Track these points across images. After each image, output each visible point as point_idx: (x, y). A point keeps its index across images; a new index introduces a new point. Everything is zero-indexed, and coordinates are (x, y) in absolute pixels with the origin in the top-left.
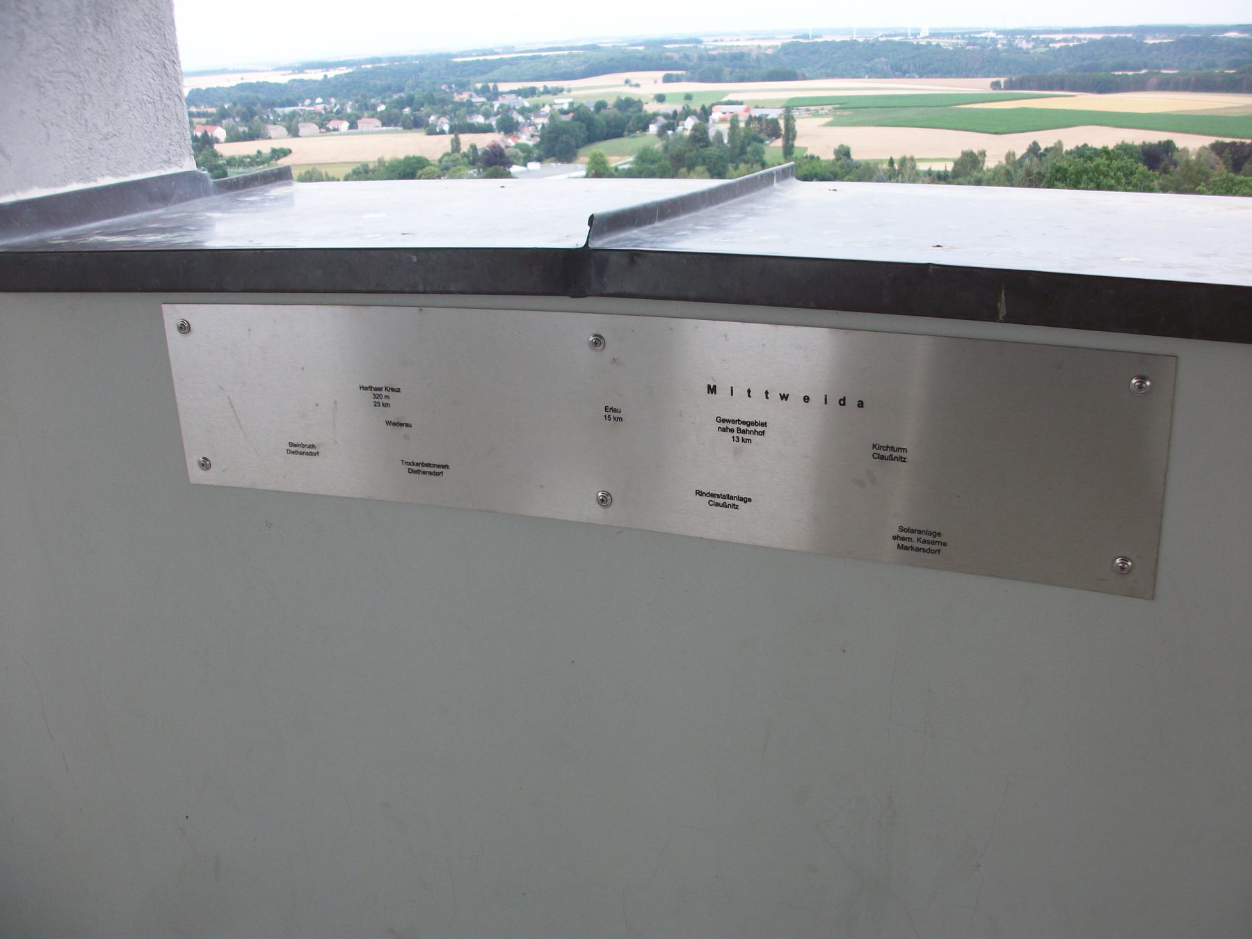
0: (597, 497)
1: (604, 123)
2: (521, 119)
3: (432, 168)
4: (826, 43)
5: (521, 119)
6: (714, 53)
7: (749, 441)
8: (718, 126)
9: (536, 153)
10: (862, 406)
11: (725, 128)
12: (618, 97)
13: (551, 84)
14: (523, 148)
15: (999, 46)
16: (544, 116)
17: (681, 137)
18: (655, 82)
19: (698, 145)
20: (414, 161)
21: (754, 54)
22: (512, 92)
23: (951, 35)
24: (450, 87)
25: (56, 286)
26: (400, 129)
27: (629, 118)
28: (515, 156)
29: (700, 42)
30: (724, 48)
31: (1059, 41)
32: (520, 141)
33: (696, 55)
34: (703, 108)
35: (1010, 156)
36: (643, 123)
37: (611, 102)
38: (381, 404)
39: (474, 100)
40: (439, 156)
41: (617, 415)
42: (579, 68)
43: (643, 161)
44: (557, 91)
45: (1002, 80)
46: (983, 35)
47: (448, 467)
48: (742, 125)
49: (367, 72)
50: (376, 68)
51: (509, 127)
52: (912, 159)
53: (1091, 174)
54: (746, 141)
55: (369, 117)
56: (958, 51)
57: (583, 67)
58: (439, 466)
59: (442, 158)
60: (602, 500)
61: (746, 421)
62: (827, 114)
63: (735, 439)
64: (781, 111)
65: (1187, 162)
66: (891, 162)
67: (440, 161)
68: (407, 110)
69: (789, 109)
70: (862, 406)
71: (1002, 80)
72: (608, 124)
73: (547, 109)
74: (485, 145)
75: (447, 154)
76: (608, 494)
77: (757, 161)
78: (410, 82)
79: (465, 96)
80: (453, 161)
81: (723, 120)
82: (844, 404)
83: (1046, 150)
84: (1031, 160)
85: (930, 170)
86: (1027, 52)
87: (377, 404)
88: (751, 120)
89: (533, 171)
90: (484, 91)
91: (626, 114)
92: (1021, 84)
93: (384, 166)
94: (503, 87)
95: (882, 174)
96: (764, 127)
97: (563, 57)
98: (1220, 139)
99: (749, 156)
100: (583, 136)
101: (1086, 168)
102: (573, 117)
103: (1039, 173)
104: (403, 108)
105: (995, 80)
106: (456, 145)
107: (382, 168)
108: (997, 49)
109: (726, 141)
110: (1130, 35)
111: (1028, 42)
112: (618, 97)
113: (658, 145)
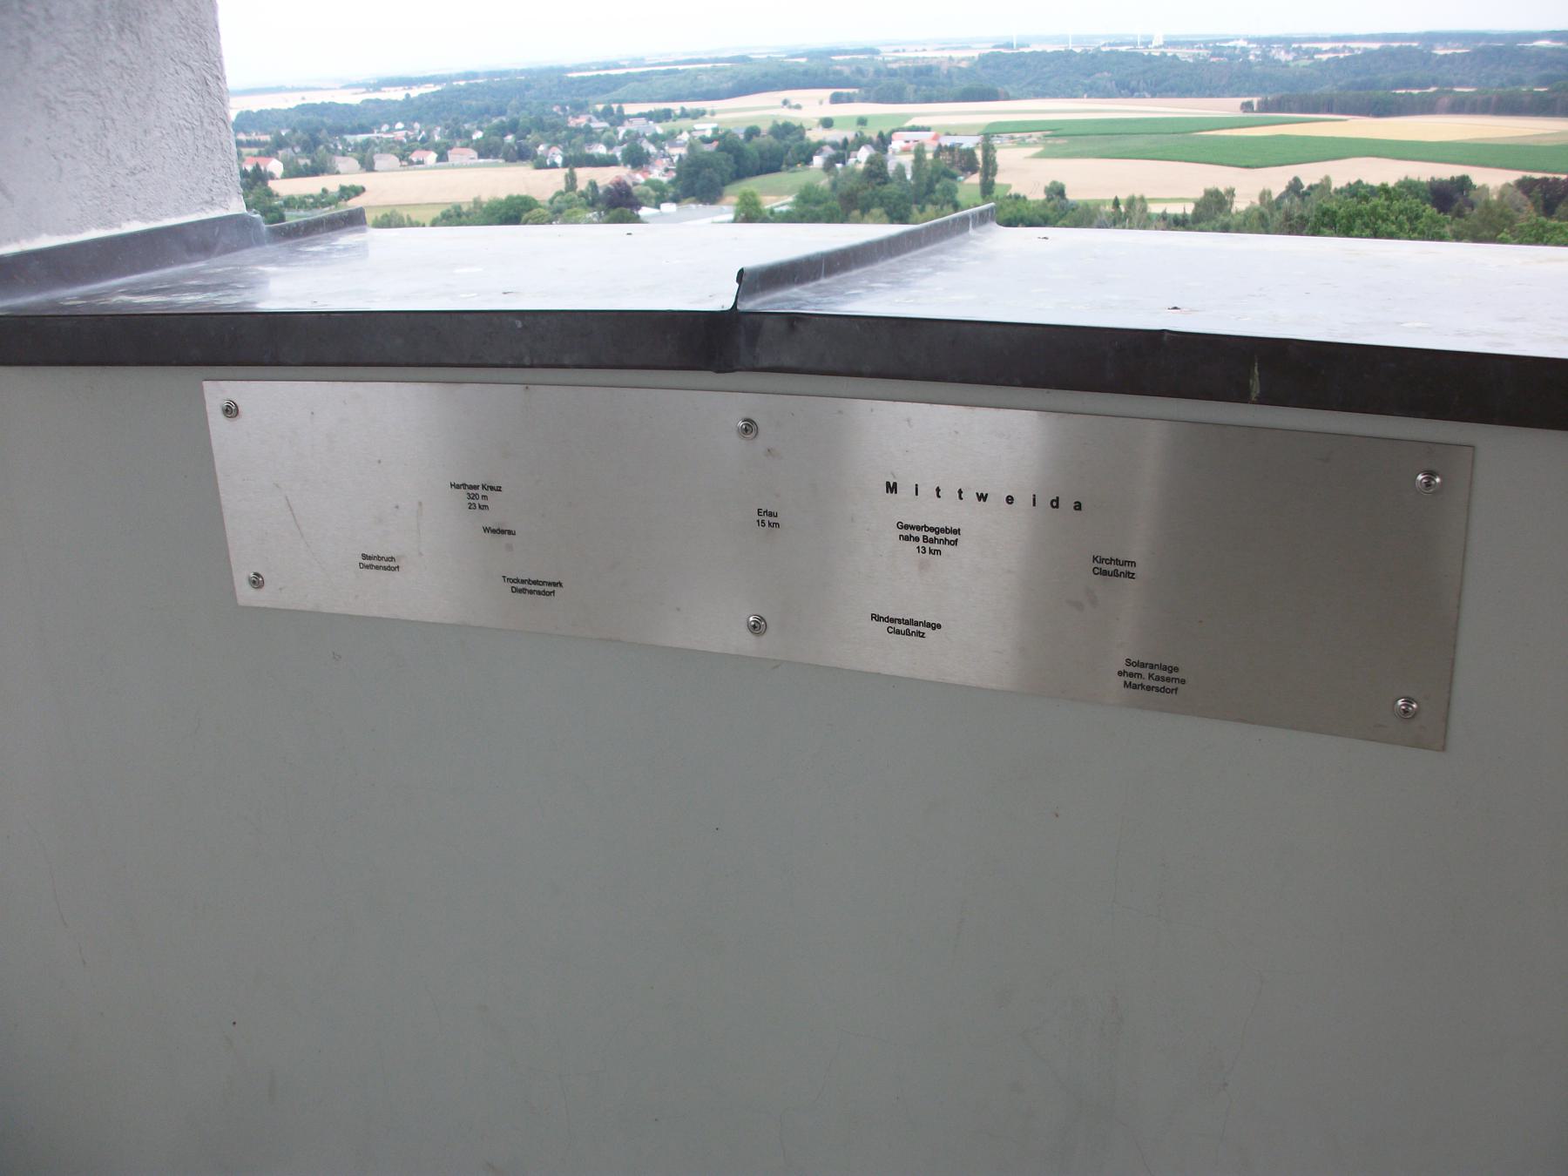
0: (748, 622)
1: (756, 154)
2: (652, 149)
3: (541, 210)
4: (1035, 54)
5: (652, 149)
6: (895, 66)
7: (938, 552)
8: (899, 158)
9: (671, 191)
10: (1080, 509)
11: (908, 160)
12: (775, 122)
13: (690, 106)
14: (655, 185)
15: (1251, 57)
16: (681, 146)
17: (853, 171)
18: (821, 103)
19: (874, 182)
20: (519, 201)
21: (944, 68)
22: (641, 115)
23: (1192, 44)
24: (564, 109)
26: (501, 161)
27: (788, 148)
28: (645, 196)
29: (876, 52)
30: (907, 60)
31: (1326, 52)
32: (651, 177)
33: (872, 69)
34: (881, 135)
35: (1265, 195)
36: (806, 154)
37: (765, 127)
38: (477, 506)
39: (593, 125)
40: (550, 195)
41: (773, 520)
42: (725, 85)
43: (806, 202)
44: (698, 114)
45: (1255, 100)
46: (1231, 44)
47: (561, 585)
48: (929, 156)
49: (460, 90)
50: (471, 85)
51: (637, 159)
52: (1142, 199)
53: (1366, 219)
54: (935, 177)
55: (462, 147)
56: (1199, 64)
57: (730, 84)
58: (550, 584)
59: (554, 198)
60: (754, 627)
62: (1035, 143)
63: (921, 550)
64: (978, 139)
65: (1487, 202)
66: (1116, 203)
67: (551, 202)
68: (510, 138)
69: (988, 137)
70: (1080, 509)
71: (1255, 100)
72: (762, 155)
73: (685, 137)
74: (607, 182)
75: (560, 193)
76: (762, 619)
77: (948, 202)
78: (513, 102)
79: (582, 121)
80: (567, 202)
81: (905, 151)
82: (1057, 507)
83: (1311, 188)
84: (1292, 201)
85: (1164, 213)
86: (1286, 65)
87: (472, 506)
88: (940, 150)
89: (668, 214)
90: (606, 114)
91: (784, 142)
92: (1278, 105)
93: (481, 207)
94: (630, 109)
95: (1104, 217)
96: (957, 159)
97: (706, 71)
98: (1528, 174)
99: (937, 196)
100: (730, 170)
101: (1360, 211)
102: (718, 147)
103: (1301, 217)
104: (505, 136)
105: (1246, 100)
106: (571, 181)
107: (478, 211)
108: (1249, 61)
109: (909, 177)
110: (1415, 44)
111: (1287, 52)
112: (775, 122)
113: (824, 182)
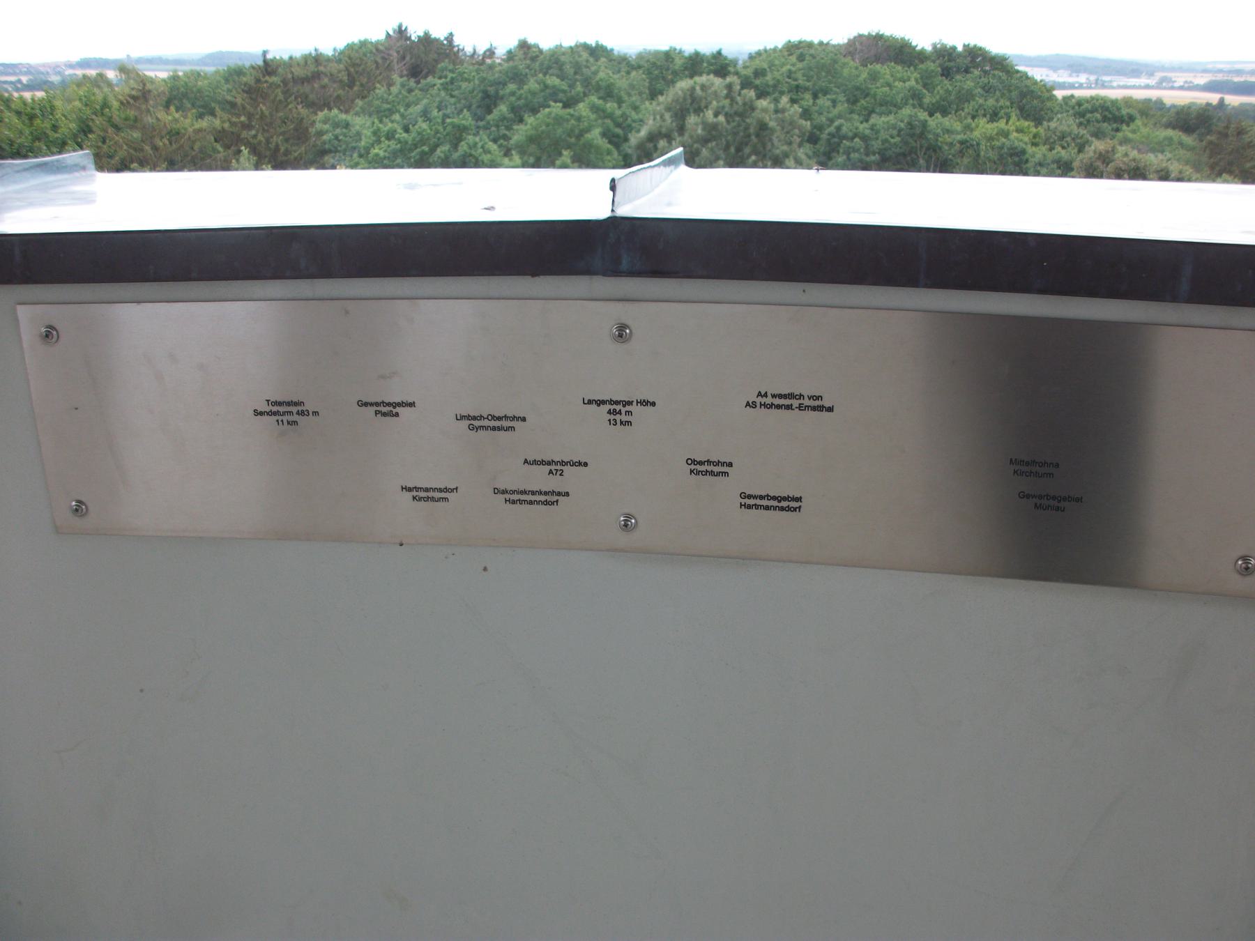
0: (71, 506)
22: (1113, 88)
23: (1205, 71)
25: (324, 270)
38: (618, 422)
41: (300, 408)
58: (440, 490)
60: (77, 510)
61: (777, 496)
